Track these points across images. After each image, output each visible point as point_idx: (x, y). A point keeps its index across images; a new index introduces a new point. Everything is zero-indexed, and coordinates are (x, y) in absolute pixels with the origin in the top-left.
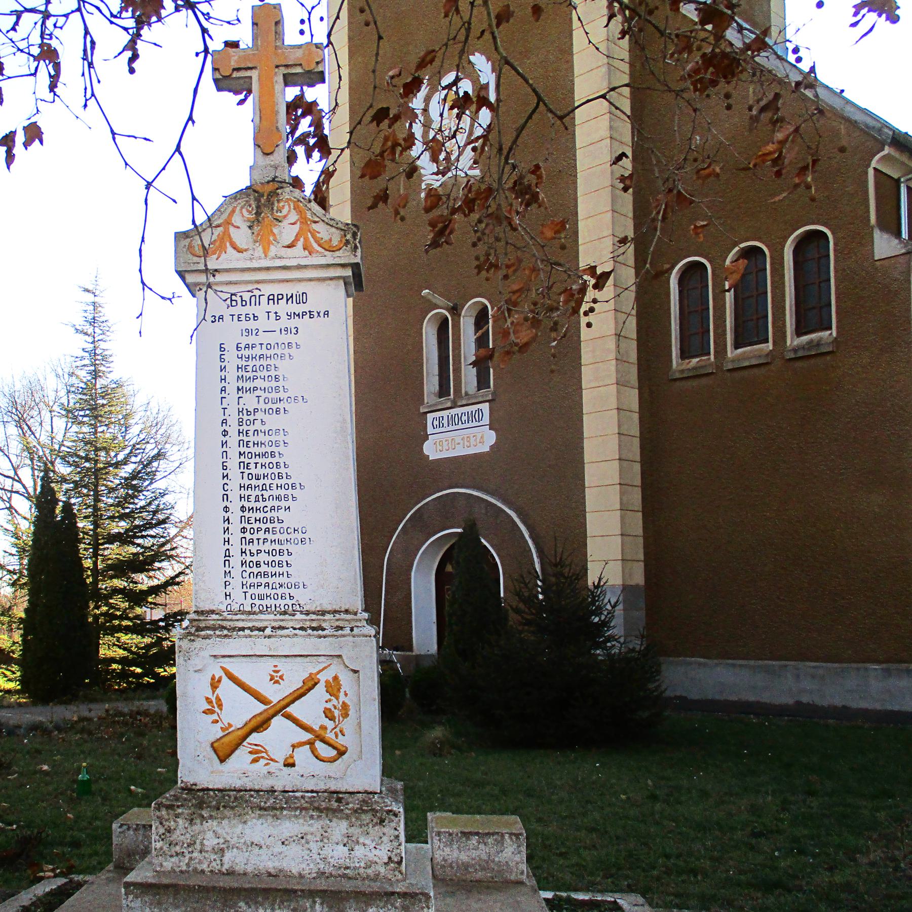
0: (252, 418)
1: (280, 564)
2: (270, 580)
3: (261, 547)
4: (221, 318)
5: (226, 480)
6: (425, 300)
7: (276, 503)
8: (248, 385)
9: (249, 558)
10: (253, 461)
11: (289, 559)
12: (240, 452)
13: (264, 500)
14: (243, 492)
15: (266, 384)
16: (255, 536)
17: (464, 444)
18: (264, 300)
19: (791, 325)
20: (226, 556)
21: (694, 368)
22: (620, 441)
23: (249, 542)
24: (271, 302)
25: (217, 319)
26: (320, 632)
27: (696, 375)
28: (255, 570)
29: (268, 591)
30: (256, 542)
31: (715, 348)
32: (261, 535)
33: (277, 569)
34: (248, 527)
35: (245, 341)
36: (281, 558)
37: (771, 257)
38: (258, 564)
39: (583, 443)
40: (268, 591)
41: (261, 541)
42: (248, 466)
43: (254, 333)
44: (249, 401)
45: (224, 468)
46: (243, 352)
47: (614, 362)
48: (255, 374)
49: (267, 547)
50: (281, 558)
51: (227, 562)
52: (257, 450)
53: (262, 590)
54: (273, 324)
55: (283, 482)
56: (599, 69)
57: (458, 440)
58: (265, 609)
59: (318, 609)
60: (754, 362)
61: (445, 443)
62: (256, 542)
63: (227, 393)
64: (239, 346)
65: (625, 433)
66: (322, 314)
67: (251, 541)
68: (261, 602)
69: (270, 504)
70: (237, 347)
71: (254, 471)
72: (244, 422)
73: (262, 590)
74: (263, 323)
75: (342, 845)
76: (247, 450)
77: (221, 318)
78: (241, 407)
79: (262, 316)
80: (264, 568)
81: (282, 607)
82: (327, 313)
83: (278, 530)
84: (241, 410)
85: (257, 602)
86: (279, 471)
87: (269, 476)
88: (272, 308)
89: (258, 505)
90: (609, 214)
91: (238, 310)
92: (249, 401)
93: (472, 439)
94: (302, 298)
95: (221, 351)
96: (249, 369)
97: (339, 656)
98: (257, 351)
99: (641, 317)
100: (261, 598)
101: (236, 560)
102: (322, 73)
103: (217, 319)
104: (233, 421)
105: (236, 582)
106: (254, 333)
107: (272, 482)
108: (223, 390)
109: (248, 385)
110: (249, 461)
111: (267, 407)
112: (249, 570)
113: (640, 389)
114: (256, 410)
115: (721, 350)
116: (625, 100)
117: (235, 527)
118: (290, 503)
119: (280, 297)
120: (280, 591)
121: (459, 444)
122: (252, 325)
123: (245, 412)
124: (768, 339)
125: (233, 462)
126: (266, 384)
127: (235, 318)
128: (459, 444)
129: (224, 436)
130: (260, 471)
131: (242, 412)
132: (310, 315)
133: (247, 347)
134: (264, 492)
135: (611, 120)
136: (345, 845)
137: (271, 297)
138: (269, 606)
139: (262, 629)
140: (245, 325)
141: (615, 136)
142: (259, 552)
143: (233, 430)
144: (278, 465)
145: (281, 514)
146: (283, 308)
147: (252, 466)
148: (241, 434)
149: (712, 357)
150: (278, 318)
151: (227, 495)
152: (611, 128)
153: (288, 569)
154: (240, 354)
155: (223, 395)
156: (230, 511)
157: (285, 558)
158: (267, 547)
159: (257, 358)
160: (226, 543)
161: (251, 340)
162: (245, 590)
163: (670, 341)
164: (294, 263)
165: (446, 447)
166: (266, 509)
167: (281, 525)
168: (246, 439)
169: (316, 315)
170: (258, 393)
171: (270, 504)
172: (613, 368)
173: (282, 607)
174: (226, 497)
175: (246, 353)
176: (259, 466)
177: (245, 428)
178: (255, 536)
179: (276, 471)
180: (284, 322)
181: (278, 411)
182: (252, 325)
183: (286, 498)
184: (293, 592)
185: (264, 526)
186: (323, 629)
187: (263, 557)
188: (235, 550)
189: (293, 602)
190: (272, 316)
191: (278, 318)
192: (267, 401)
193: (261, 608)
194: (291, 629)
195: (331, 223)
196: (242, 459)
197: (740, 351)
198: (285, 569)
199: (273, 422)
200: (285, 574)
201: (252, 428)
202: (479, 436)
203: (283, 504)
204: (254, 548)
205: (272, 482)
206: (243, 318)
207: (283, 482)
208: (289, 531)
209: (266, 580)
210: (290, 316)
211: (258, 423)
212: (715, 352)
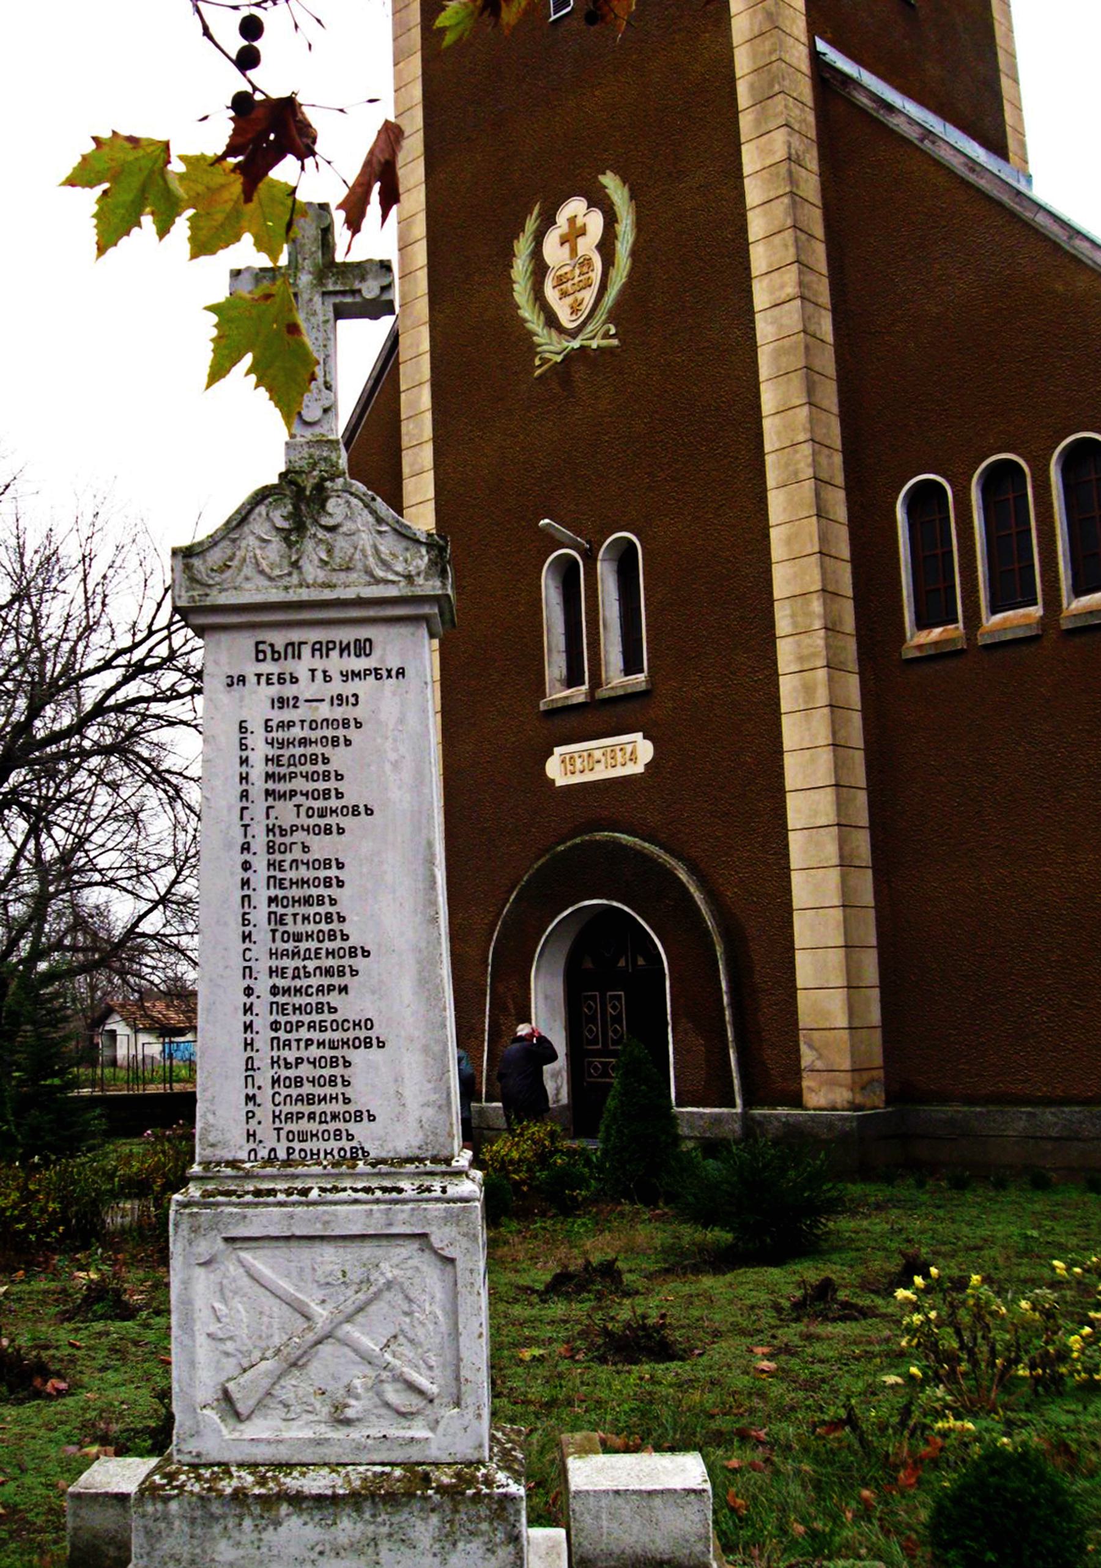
0: (288, 840)
1: (332, 1081)
2: (317, 1109)
3: (304, 1054)
4: (242, 679)
5: (247, 945)
6: (544, 532)
7: (326, 981)
8: (282, 787)
9: (279, 840)
10: (290, 910)
11: (347, 1072)
12: (270, 968)
13: (308, 975)
14: (270, 785)
15: (311, 786)
16: (293, 1036)
17: (606, 762)
18: (306, 651)
19: (1066, 579)
20: (247, 1070)
21: (936, 644)
22: (835, 756)
23: (284, 1045)
24: (317, 653)
25: (235, 680)
26: (394, 1195)
27: (939, 655)
28: (294, 1092)
29: (314, 1126)
30: (294, 1044)
31: (964, 612)
32: (304, 1033)
33: (328, 1090)
34: (282, 1019)
35: (278, 716)
36: (333, 1071)
37: (1033, 477)
38: (299, 1082)
39: (782, 760)
40: (314, 1126)
41: (302, 1044)
42: (281, 920)
43: (292, 703)
44: (286, 814)
45: (245, 922)
46: (274, 734)
47: (822, 633)
48: (292, 769)
49: (314, 1052)
50: (333, 1071)
51: (250, 1079)
52: (296, 892)
53: (304, 1125)
54: (318, 689)
55: (338, 943)
56: (781, 200)
57: (598, 754)
58: (309, 1157)
59: (392, 1155)
60: (1021, 634)
61: (578, 761)
62: (294, 1044)
63: (252, 887)
64: (270, 723)
65: (842, 743)
66: (394, 673)
67: (287, 1044)
68: (303, 1145)
69: (315, 981)
70: (267, 726)
71: (290, 928)
72: (276, 847)
73: (304, 1125)
74: (305, 689)
75: (430, 1555)
76: (281, 893)
77: (242, 679)
78: (271, 822)
79: (303, 674)
80: (307, 1089)
81: (335, 1153)
82: (401, 672)
83: (328, 1024)
84: (275, 1059)
85: (297, 1146)
86: (330, 926)
87: (315, 936)
88: (319, 664)
89: (298, 983)
90: (805, 410)
91: (268, 667)
92: (286, 814)
93: (619, 754)
94: (363, 648)
95: (242, 733)
96: (284, 761)
97: (424, 1236)
98: (297, 732)
99: (857, 561)
100: (303, 1137)
101: (264, 1078)
102: (391, 303)
103: (235, 680)
104: (259, 843)
105: (264, 1112)
106: (292, 703)
107: (319, 945)
108: (244, 795)
109: (282, 787)
110: (283, 911)
111: (312, 822)
112: (284, 1092)
113: (861, 674)
114: (294, 829)
115: (973, 620)
116: (824, 312)
117: (262, 1023)
118: (346, 980)
119: (331, 646)
120: (332, 1126)
121: (598, 762)
122: (289, 691)
123: (277, 831)
124: (1036, 599)
125: (260, 914)
126: (311, 786)
127: (263, 679)
128: (598, 762)
129: (248, 996)
130: (301, 928)
131: (277, 1062)
132: (376, 674)
133: (281, 725)
134: (307, 963)
135: (800, 273)
136: (435, 1555)
137: (317, 646)
138: (315, 1151)
139: (305, 1192)
140: (275, 690)
141: (807, 294)
142: (299, 1061)
143: (260, 863)
144: (329, 917)
145: (334, 999)
146: (336, 663)
147: (289, 919)
148: (277, 1120)
149: (961, 625)
150: (327, 678)
151: (250, 968)
152: (801, 284)
153: (344, 1090)
154: (270, 735)
155: (245, 804)
156: (256, 994)
157: (332, 784)
158: (314, 1052)
159: (296, 743)
160: (249, 1048)
161: (287, 715)
162: (277, 1125)
163: (901, 600)
164: (349, 594)
165: (579, 766)
166: (310, 991)
167: (333, 1017)
168: (280, 875)
169: (385, 674)
170: (298, 799)
171: (315, 981)
172: (821, 643)
173: (335, 1153)
174: (248, 971)
175: (280, 735)
176: (299, 918)
177: (278, 857)
178: (293, 1036)
179: (324, 926)
180: (338, 686)
181: (328, 830)
182: (289, 691)
183: (341, 973)
184: (352, 1127)
185: (306, 1019)
186: (400, 1191)
187: (305, 1070)
188: (263, 1059)
189: (354, 1143)
190: (319, 675)
191: (327, 678)
192: (310, 813)
193: (303, 1154)
194: (350, 1192)
195: (405, 535)
196: (273, 908)
197: (999, 617)
198: (339, 1089)
199: (321, 847)
200: (340, 1097)
201: (289, 857)
202: (629, 748)
203: (336, 981)
204: (291, 1055)
205: (319, 945)
206: (275, 679)
207: (338, 943)
208: (346, 1025)
209: (312, 1108)
210: (346, 676)
211: (296, 849)
212: (965, 617)
